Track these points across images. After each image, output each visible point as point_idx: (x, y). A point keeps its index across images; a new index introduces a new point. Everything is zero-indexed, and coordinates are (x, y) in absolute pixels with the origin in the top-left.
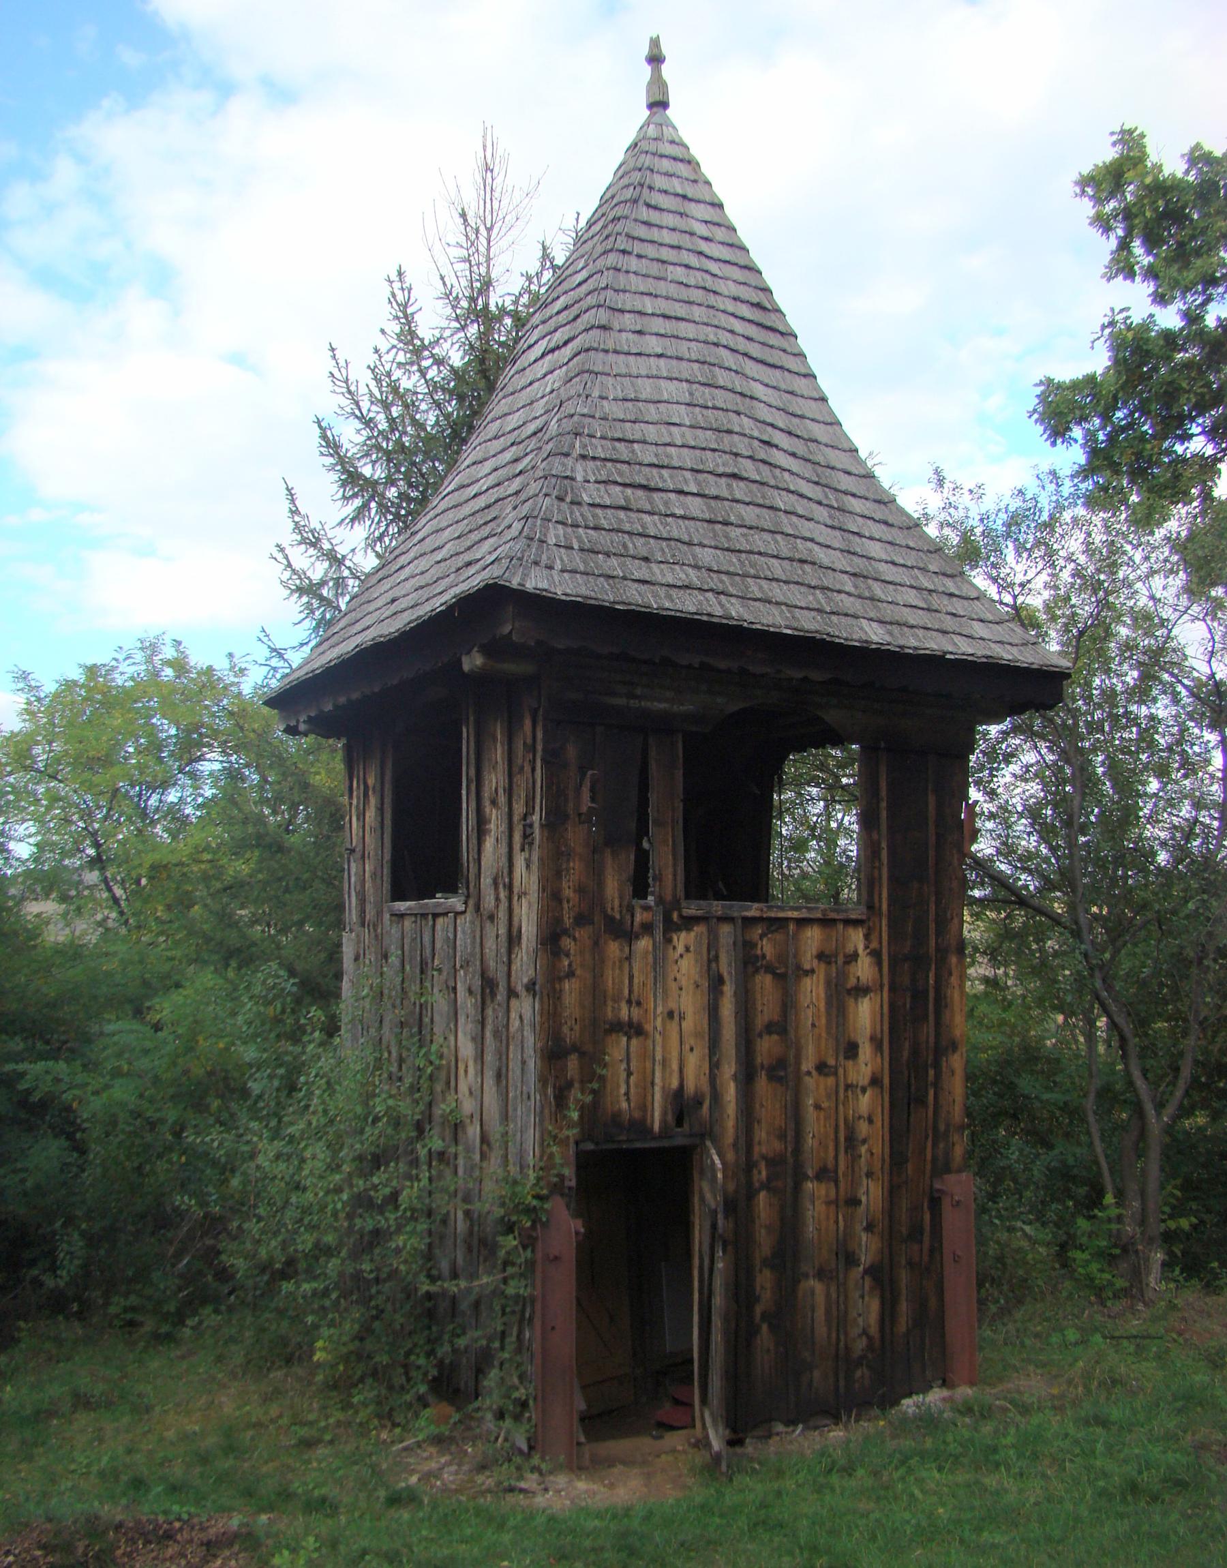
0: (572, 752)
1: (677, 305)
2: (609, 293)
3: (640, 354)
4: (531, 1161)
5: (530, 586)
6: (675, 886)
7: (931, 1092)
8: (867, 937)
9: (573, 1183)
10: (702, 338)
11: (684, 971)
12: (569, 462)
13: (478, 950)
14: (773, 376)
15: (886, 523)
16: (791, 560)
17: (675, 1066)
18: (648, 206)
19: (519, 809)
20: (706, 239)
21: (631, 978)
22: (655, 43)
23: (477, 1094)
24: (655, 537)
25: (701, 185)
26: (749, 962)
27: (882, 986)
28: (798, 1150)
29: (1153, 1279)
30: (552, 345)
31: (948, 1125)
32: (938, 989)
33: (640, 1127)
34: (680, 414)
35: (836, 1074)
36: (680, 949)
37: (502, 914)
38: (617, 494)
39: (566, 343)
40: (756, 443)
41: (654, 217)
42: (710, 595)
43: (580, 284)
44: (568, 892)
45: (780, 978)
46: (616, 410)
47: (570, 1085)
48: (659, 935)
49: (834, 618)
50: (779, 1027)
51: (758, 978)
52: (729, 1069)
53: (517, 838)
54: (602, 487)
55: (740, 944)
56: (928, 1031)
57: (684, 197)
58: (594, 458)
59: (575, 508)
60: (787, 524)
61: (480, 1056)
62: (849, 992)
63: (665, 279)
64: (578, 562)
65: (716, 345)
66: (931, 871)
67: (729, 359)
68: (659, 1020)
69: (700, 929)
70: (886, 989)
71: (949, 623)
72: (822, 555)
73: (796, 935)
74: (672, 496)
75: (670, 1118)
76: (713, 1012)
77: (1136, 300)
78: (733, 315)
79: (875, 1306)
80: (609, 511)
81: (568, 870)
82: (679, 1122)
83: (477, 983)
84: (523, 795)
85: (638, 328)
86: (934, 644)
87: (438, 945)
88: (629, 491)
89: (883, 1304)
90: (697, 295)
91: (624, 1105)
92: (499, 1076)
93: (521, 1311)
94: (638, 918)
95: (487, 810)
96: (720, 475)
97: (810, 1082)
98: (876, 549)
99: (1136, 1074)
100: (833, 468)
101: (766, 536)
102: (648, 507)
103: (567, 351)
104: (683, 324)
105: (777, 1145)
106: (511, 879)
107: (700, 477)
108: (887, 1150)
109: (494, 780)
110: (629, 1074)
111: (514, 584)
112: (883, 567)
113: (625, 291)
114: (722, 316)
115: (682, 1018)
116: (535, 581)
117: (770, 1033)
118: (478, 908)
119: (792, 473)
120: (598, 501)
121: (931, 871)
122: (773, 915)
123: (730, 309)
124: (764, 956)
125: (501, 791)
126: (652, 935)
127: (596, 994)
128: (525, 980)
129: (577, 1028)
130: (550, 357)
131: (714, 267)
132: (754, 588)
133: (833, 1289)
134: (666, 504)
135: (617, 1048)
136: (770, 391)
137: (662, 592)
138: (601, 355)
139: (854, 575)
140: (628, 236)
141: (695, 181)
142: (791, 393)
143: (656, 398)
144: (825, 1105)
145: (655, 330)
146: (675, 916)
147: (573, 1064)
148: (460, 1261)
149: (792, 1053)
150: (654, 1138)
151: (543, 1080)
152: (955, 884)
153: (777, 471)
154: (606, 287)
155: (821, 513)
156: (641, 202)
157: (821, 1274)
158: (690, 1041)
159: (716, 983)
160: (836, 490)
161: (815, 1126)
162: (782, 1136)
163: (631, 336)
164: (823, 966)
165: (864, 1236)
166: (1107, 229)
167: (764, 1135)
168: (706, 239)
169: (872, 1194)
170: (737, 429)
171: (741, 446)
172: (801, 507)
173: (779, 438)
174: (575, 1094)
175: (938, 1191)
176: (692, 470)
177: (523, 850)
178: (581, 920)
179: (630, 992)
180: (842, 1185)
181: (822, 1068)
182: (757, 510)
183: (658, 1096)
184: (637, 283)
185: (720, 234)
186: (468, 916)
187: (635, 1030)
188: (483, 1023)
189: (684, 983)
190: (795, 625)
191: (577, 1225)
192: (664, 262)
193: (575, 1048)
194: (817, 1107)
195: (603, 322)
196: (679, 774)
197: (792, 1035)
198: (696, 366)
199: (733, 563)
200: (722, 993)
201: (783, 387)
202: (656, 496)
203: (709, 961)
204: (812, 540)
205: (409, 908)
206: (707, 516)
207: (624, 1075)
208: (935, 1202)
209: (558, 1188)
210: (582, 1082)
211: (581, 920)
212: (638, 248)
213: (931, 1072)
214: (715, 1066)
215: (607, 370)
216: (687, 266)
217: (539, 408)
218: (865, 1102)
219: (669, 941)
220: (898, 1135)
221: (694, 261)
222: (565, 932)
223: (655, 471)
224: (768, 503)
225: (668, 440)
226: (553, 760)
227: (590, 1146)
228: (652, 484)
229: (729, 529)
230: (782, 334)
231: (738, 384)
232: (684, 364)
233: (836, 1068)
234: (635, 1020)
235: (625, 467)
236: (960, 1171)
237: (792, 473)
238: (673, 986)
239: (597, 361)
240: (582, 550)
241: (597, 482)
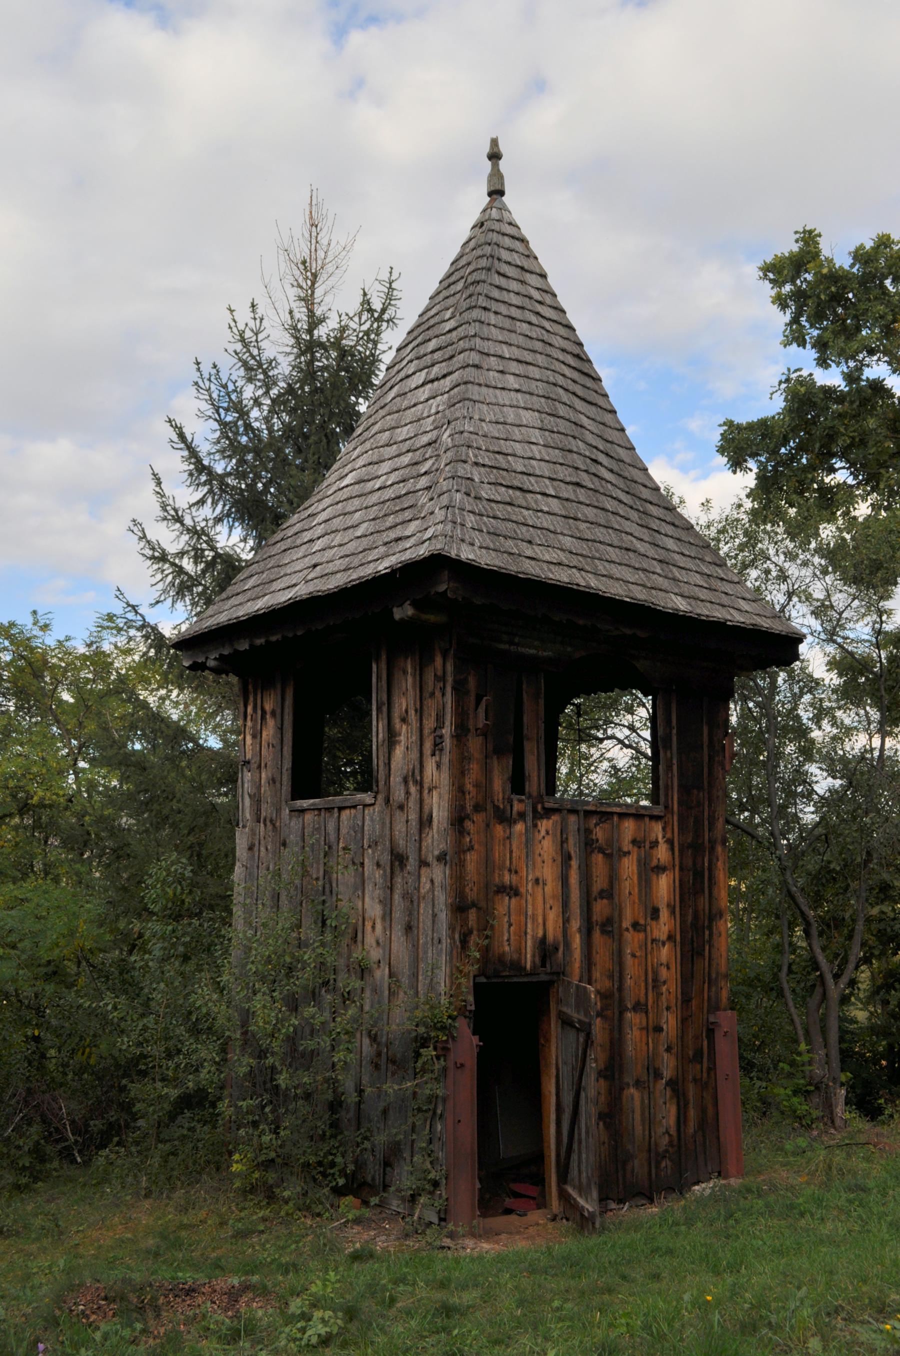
0: (472, 683)
1: (526, 353)
2: (478, 340)
3: (503, 389)
4: (442, 988)
5: (463, 556)
6: (539, 785)
7: (707, 947)
8: (664, 829)
9: (473, 1008)
10: (545, 379)
11: (545, 848)
12: (467, 467)
13: (388, 832)
14: (592, 411)
15: (673, 524)
16: (620, 548)
17: (540, 920)
18: (499, 273)
19: (430, 723)
20: (540, 302)
21: (511, 852)
22: (494, 142)
23: (385, 944)
24: (533, 526)
25: (532, 259)
26: (589, 845)
27: (674, 866)
28: (620, 989)
29: (840, 1110)
30: (432, 376)
31: (717, 973)
32: (710, 870)
33: (517, 966)
34: (536, 435)
35: (645, 931)
36: (543, 833)
37: (412, 804)
38: (503, 494)
39: (444, 376)
40: (588, 461)
41: (503, 282)
42: (574, 570)
43: (450, 331)
44: (469, 787)
45: (608, 856)
46: (494, 430)
47: (471, 932)
48: (530, 823)
49: (653, 592)
50: (608, 894)
51: (594, 856)
52: (575, 924)
53: (428, 746)
54: (492, 487)
55: (582, 829)
56: (703, 902)
57: (522, 268)
58: (484, 465)
59: (478, 502)
60: (615, 522)
61: (387, 915)
62: (653, 869)
63: (515, 332)
64: (488, 541)
65: (555, 385)
66: (706, 783)
67: (565, 397)
68: (530, 885)
69: (555, 818)
70: (677, 868)
71: (725, 600)
72: (639, 546)
73: (618, 826)
74: (539, 496)
75: (537, 960)
76: (564, 880)
77: (804, 360)
78: (563, 362)
79: (673, 1110)
80: (501, 506)
81: (469, 770)
82: (543, 965)
83: (386, 858)
84: (433, 714)
85: (501, 368)
86: (719, 614)
87: (344, 831)
88: (511, 491)
89: (679, 1109)
90: (538, 346)
91: (507, 948)
92: (409, 928)
93: (431, 1109)
94: (515, 808)
95: (398, 726)
96: (567, 483)
97: (628, 936)
98: (670, 544)
99: (818, 951)
100: (636, 482)
101: (602, 529)
102: (524, 504)
103: (448, 382)
104: (531, 368)
105: (607, 984)
106: (422, 778)
107: (556, 483)
108: (679, 990)
109: (404, 702)
110: (510, 925)
111: (453, 554)
112: (677, 557)
113: (488, 339)
114: (557, 363)
115: (544, 884)
116: (466, 554)
117: (602, 898)
118: (387, 801)
119: (613, 484)
120: (492, 497)
121: (706, 783)
122: (603, 809)
123: (561, 358)
124: (597, 840)
125: (412, 712)
126: (525, 821)
127: (488, 863)
128: (436, 853)
129: (475, 889)
130: (430, 385)
131: (547, 324)
132: (601, 567)
133: (646, 1096)
134: (536, 502)
135: (503, 904)
136: (591, 422)
137: (545, 566)
138: (476, 387)
139: (660, 561)
140: (487, 296)
141: (528, 256)
142: (603, 424)
143: (518, 422)
144: (638, 954)
145: (513, 371)
146: (539, 807)
147: (472, 915)
148: (365, 1080)
149: (616, 914)
150: (527, 975)
151: (452, 928)
152: (720, 793)
153: (603, 482)
154: (475, 336)
155: (634, 515)
156: (493, 270)
157: (638, 1084)
158: (550, 902)
159: (566, 858)
160: (640, 498)
161: (632, 968)
162: (611, 977)
163: (496, 374)
164: (636, 849)
165: (665, 1055)
166: (784, 306)
167: (598, 974)
168: (540, 302)
169: (670, 1022)
170: (575, 449)
171: (579, 462)
172: (622, 510)
173: (602, 458)
174: (474, 939)
175: (712, 1023)
176: (550, 478)
177: (433, 755)
178: (477, 808)
179: (511, 863)
180: (650, 1015)
181: (635, 925)
182: (595, 510)
183: (529, 943)
184: (495, 333)
185: (548, 299)
186: (377, 808)
187: (514, 891)
188: (391, 889)
189: (545, 857)
190: (631, 595)
191: (475, 1040)
192: (513, 319)
193: (474, 905)
194: (633, 956)
195: (477, 362)
196: (542, 702)
197: (616, 900)
198: (543, 400)
199: (583, 548)
200: (570, 866)
201: (598, 419)
202: (529, 496)
203: (562, 842)
204: (631, 534)
205: (312, 804)
206: (563, 513)
207: (506, 926)
208: (711, 1032)
209: (462, 1011)
210: (478, 930)
211: (477, 808)
212: (494, 306)
213: (707, 933)
214: (566, 921)
215: (482, 399)
216: (530, 323)
217: (428, 424)
218: (665, 952)
219: (535, 826)
220: (687, 978)
221: (534, 319)
222: (468, 817)
223: (525, 477)
224: (601, 505)
225: (530, 455)
226: (459, 689)
227: (483, 980)
228: (525, 488)
229: (579, 523)
230: (593, 379)
231: (572, 415)
232: (535, 398)
233: (645, 926)
234: (514, 883)
235: (505, 473)
236: (725, 1010)
237: (613, 484)
238: (539, 859)
239: (474, 392)
240: (489, 533)
241: (489, 483)
